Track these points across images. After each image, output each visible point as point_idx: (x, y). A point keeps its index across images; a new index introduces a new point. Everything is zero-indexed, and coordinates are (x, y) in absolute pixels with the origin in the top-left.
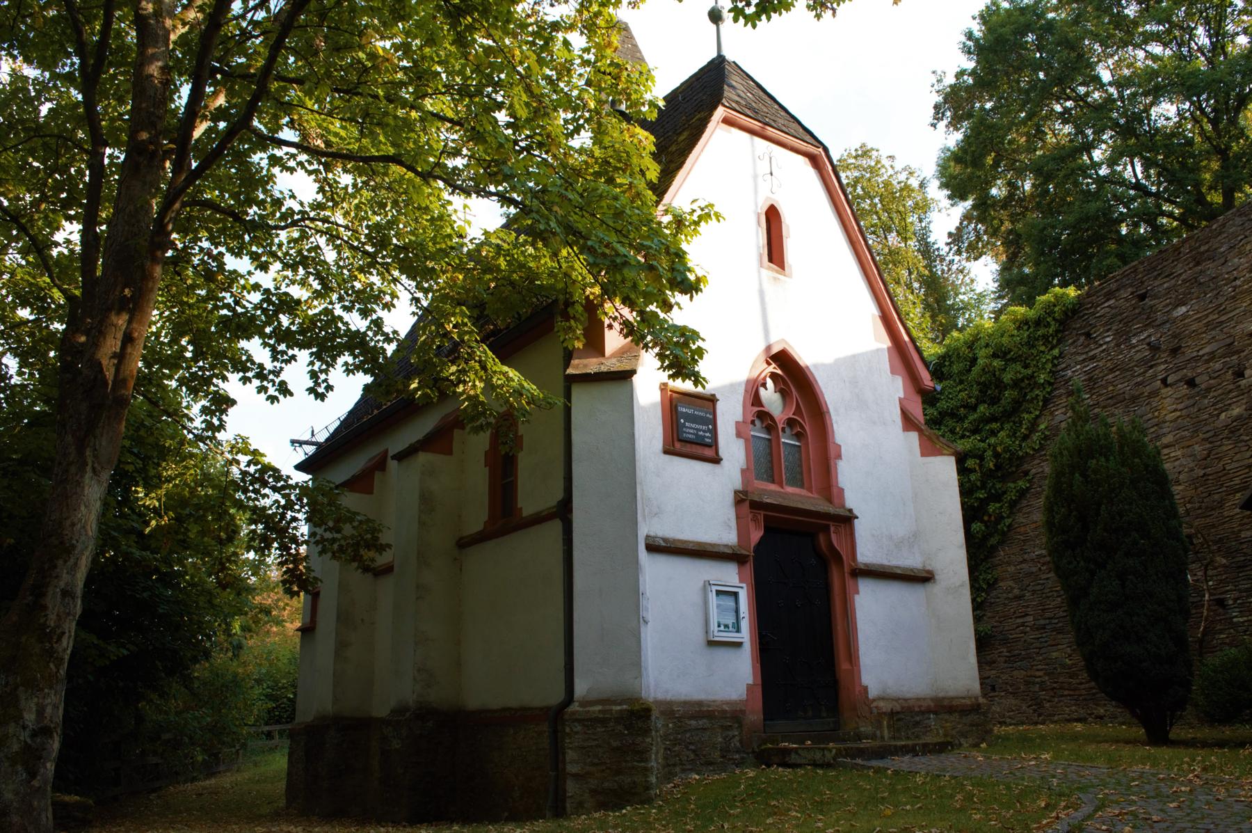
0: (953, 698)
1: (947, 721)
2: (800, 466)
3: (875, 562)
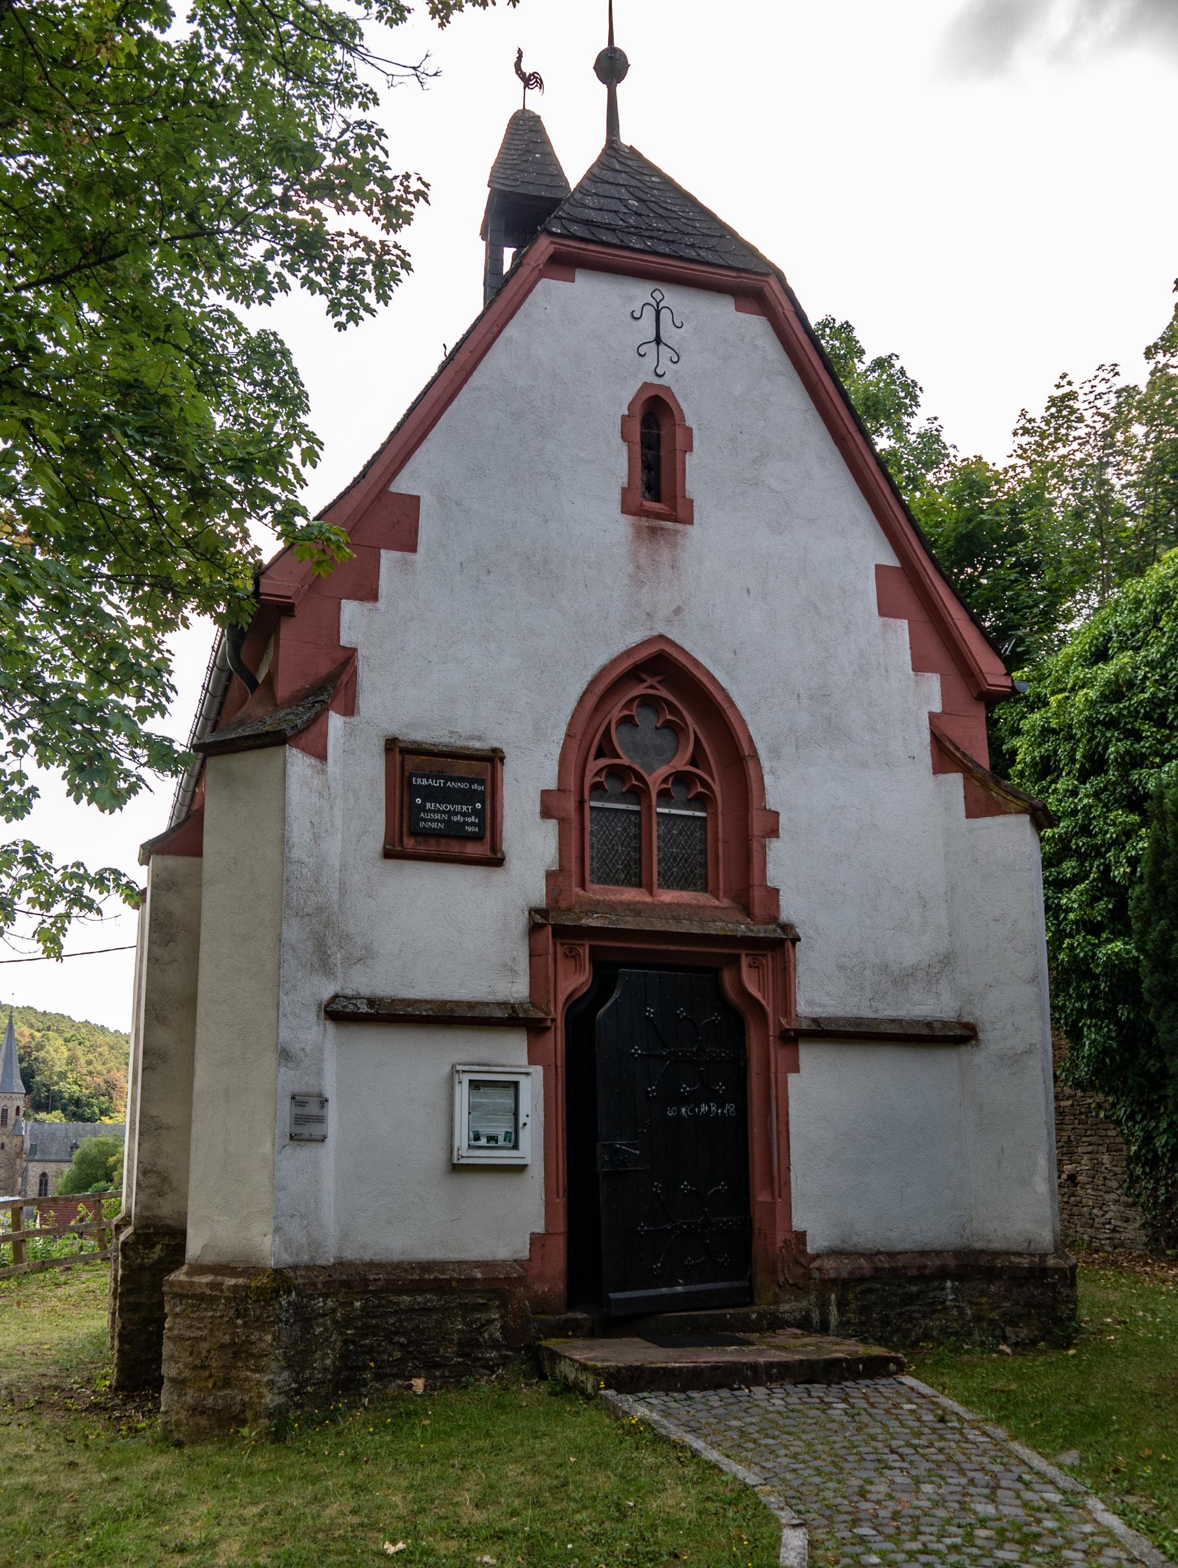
0: (996, 1254)
1: (982, 1293)
2: (704, 852)
3: (841, 1013)
